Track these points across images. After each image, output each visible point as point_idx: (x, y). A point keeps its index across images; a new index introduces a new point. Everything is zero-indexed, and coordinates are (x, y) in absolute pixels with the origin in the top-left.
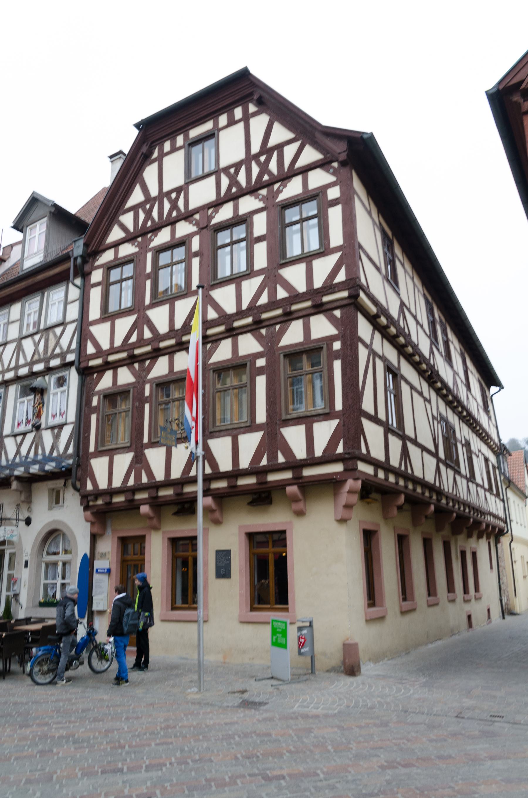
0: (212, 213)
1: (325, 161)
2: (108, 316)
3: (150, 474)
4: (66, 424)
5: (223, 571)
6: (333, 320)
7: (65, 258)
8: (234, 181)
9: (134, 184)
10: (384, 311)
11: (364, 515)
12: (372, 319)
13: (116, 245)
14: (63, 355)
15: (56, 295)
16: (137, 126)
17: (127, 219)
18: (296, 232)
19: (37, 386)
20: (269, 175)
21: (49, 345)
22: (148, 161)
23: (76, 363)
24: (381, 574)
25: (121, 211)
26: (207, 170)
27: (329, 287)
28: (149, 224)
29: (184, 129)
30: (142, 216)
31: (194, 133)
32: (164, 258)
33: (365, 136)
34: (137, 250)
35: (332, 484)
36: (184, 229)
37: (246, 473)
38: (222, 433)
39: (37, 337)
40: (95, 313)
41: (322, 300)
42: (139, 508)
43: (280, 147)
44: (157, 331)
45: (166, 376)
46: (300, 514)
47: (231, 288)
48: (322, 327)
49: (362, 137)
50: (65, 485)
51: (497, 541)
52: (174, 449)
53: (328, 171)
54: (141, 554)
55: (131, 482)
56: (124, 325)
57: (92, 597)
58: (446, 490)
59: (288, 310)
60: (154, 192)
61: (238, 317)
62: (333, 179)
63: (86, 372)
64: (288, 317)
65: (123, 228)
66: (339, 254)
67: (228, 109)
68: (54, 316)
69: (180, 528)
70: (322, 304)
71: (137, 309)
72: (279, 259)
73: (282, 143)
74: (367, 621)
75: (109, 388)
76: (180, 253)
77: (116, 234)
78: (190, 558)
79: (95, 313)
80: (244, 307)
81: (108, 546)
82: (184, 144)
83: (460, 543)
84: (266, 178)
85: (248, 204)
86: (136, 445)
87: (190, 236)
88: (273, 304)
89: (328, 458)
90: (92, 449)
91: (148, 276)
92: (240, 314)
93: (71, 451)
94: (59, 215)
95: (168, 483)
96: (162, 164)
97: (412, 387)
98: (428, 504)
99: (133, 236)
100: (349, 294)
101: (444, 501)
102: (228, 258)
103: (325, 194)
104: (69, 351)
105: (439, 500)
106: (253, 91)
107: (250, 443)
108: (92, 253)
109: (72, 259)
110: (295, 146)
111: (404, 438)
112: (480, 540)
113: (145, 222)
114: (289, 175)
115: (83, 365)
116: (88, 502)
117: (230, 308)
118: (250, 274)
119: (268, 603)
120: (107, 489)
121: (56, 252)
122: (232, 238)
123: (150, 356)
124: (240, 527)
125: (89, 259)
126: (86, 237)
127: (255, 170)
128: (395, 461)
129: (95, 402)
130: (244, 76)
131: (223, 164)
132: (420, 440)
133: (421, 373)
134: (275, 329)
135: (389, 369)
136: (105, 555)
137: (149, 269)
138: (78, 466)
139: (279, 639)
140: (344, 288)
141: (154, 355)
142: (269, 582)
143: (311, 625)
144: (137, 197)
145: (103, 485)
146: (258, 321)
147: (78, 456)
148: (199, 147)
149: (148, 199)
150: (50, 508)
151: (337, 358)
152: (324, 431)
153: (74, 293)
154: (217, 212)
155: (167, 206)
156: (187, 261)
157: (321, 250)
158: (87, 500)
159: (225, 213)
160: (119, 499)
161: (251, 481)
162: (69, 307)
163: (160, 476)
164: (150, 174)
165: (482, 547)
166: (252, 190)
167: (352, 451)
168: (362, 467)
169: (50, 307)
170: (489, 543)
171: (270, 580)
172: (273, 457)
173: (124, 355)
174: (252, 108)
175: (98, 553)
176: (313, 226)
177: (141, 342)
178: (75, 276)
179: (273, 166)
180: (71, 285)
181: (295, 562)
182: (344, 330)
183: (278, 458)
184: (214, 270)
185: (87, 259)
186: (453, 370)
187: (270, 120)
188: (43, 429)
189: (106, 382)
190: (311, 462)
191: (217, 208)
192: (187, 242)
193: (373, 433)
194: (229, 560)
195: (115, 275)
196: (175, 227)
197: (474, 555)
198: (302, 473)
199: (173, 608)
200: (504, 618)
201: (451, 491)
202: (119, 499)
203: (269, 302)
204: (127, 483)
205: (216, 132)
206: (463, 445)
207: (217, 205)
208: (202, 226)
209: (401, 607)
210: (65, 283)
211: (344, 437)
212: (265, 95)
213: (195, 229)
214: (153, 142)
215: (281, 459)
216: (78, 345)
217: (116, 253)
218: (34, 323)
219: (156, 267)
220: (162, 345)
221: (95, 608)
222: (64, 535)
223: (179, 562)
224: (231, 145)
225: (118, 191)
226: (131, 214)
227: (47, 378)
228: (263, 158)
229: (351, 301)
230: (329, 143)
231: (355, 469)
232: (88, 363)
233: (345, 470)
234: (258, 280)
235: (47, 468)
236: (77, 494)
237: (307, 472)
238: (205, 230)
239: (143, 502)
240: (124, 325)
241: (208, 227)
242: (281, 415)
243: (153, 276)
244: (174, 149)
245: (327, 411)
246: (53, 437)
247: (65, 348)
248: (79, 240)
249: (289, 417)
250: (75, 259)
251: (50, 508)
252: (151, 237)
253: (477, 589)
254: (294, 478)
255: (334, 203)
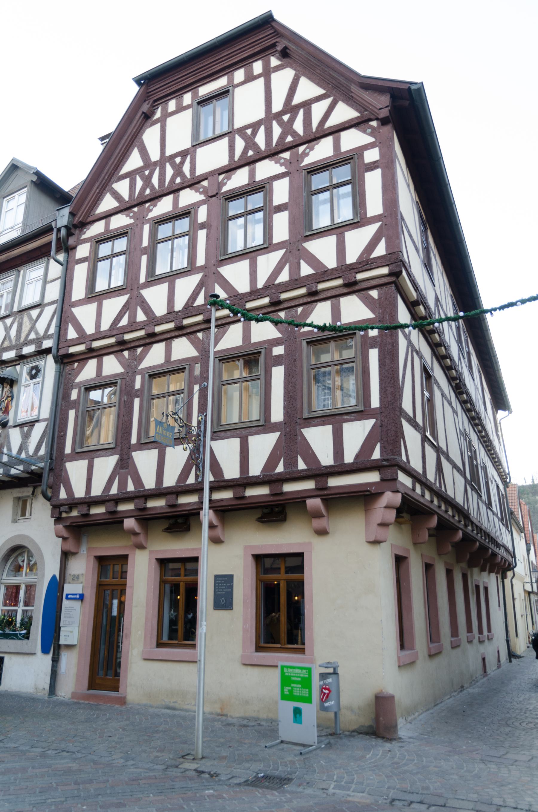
0: (223, 179)
1: (362, 119)
2: (94, 296)
3: (138, 481)
4: (37, 421)
5: (223, 600)
6: (369, 302)
7: (47, 230)
8: (250, 143)
9: (131, 148)
10: (422, 301)
11: (396, 539)
12: (411, 305)
13: (107, 216)
14: (38, 341)
15: (34, 273)
16: (138, 81)
17: (122, 187)
18: (324, 202)
19: (6, 377)
20: (292, 136)
21: (23, 330)
22: (150, 121)
23: (54, 351)
24: (411, 611)
25: (114, 178)
26: (218, 132)
27: (365, 262)
28: (148, 192)
29: (192, 86)
30: (139, 183)
31: (205, 90)
32: (165, 230)
33: (413, 87)
34: (132, 221)
35: (364, 497)
36: (188, 197)
37: (256, 482)
38: (229, 433)
39: (9, 321)
40: (79, 291)
41: (356, 277)
42: (122, 522)
43: (307, 105)
44: (153, 313)
45: (162, 365)
46: (322, 532)
47: (244, 265)
48: (354, 310)
49: (409, 88)
50: (33, 493)
51: (504, 577)
52: (169, 450)
53: (364, 132)
54: (121, 578)
55: (114, 490)
56: (113, 306)
57: (60, 628)
58: (472, 515)
59: (314, 289)
60: (155, 156)
61: (252, 298)
62: (371, 140)
63: (66, 361)
64: (314, 297)
65: (117, 196)
66: (377, 225)
67: (245, 62)
68: (31, 296)
69: (176, 547)
70: (355, 283)
71: (129, 289)
72: (304, 230)
73: (310, 100)
74: (399, 666)
75: (92, 379)
76: (183, 225)
77: (108, 203)
78: (181, 584)
79: (79, 291)
80: (260, 285)
81: (82, 567)
82: (192, 103)
83: (475, 577)
84: (289, 139)
85: (266, 169)
86: (122, 447)
87: (196, 205)
88: (295, 282)
89: (361, 466)
90: (68, 450)
91: (145, 251)
92: (255, 294)
93: (42, 452)
94: (44, 186)
95: (159, 492)
96: (165, 125)
97: (443, 395)
98: (457, 529)
99: (128, 205)
100: (390, 270)
101: (470, 528)
102: (241, 232)
103: (362, 157)
104: (46, 336)
105: (466, 526)
106: (277, 42)
107: (262, 446)
108: (78, 225)
109: (55, 230)
110: (325, 103)
111: (437, 449)
112: (491, 574)
113: (143, 189)
114: (317, 136)
115: (62, 352)
116: (60, 513)
117: (242, 286)
118: (267, 247)
119: (279, 643)
120: (85, 498)
121: (36, 225)
122: (246, 206)
123: (143, 342)
124: (246, 548)
125: (75, 231)
126: (73, 205)
127: (277, 131)
128: (431, 476)
129: (74, 395)
130: (266, 22)
131: (238, 124)
132: (451, 455)
133: (450, 379)
134: (297, 311)
135: (425, 370)
136: (78, 577)
137: (145, 243)
138: (51, 470)
139: (292, 688)
140: (384, 264)
141: (148, 341)
142: (279, 616)
143: (335, 673)
144: (134, 161)
145: (79, 492)
146: (274, 303)
147: (51, 459)
148: (209, 108)
149: (148, 164)
150: (15, 521)
151: (373, 347)
152: (356, 434)
153: (55, 269)
154: (229, 178)
155: (169, 171)
156: (191, 234)
157: (356, 221)
158: (58, 511)
159: (240, 179)
160: (98, 510)
161: (263, 491)
162: (48, 286)
163: (149, 483)
164: (151, 136)
165: (491, 580)
166: (272, 154)
167: (392, 457)
168: (402, 478)
169: (26, 286)
170: (497, 577)
171: (281, 612)
172: (291, 463)
173: (112, 340)
174: (274, 62)
175: (70, 575)
176: (345, 196)
177: (133, 326)
178: (58, 250)
179: (298, 126)
180: (52, 261)
181: (314, 592)
182: (383, 313)
183: (297, 464)
184: (224, 245)
185: (73, 231)
186: (475, 384)
187: (296, 75)
188: (10, 427)
189: (88, 371)
190: (340, 470)
191: (229, 173)
192: (193, 211)
193: (411, 437)
194: (231, 587)
195: (105, 249)
196: (179, 196)
197: (486, 589)
198: (327, 483)
199: (160, 645)
200: (510, 661)
201: (475, 517)
202: (98, 510)
203: (290, 280)
204: (109, 492)
205: (230, 88)
206: (481, 467)
207: (229, 170)
208: (210, 195)
209: (429, 649)
210: (45, 259)
211: (381, 440)
212: (291, 46)
213: (202, 197)
214: (155, 101)
215: (302, 465)
216: (58, 328)
217: (107, 225)
218: (7, 306)
219: (155, 241)
220: (158, 329)
221: (62, 641)
222: (29, 551)
223: (168, 587)
224: (248, 102)
225: (112, 155)
226: (127, 181)
227: (18, 367)
228: (286, 118)
229: (393, 279)
230: (367, 97)
231: (395, 479)
232: (68, 350)
233: (382, 480)
234: (277, 256)
235: (13, 471)
236: (48, 503)
237: (334, 482)
238: (214, 198)
239: (128, 514)
240: (113, 306)
241: (218, 196)
242: (302, 412)
243: (150, 250)
244: (180, 109)
245: (361, 408)
246: (22, 437)
247: (41, 332)
248: (63, 221)
249: (312, 415)
250: (59, 230)
251: (15, 521)
252: (149, 206)
253: (489, 630)
254: (317, 489)
255: (372, 166)
